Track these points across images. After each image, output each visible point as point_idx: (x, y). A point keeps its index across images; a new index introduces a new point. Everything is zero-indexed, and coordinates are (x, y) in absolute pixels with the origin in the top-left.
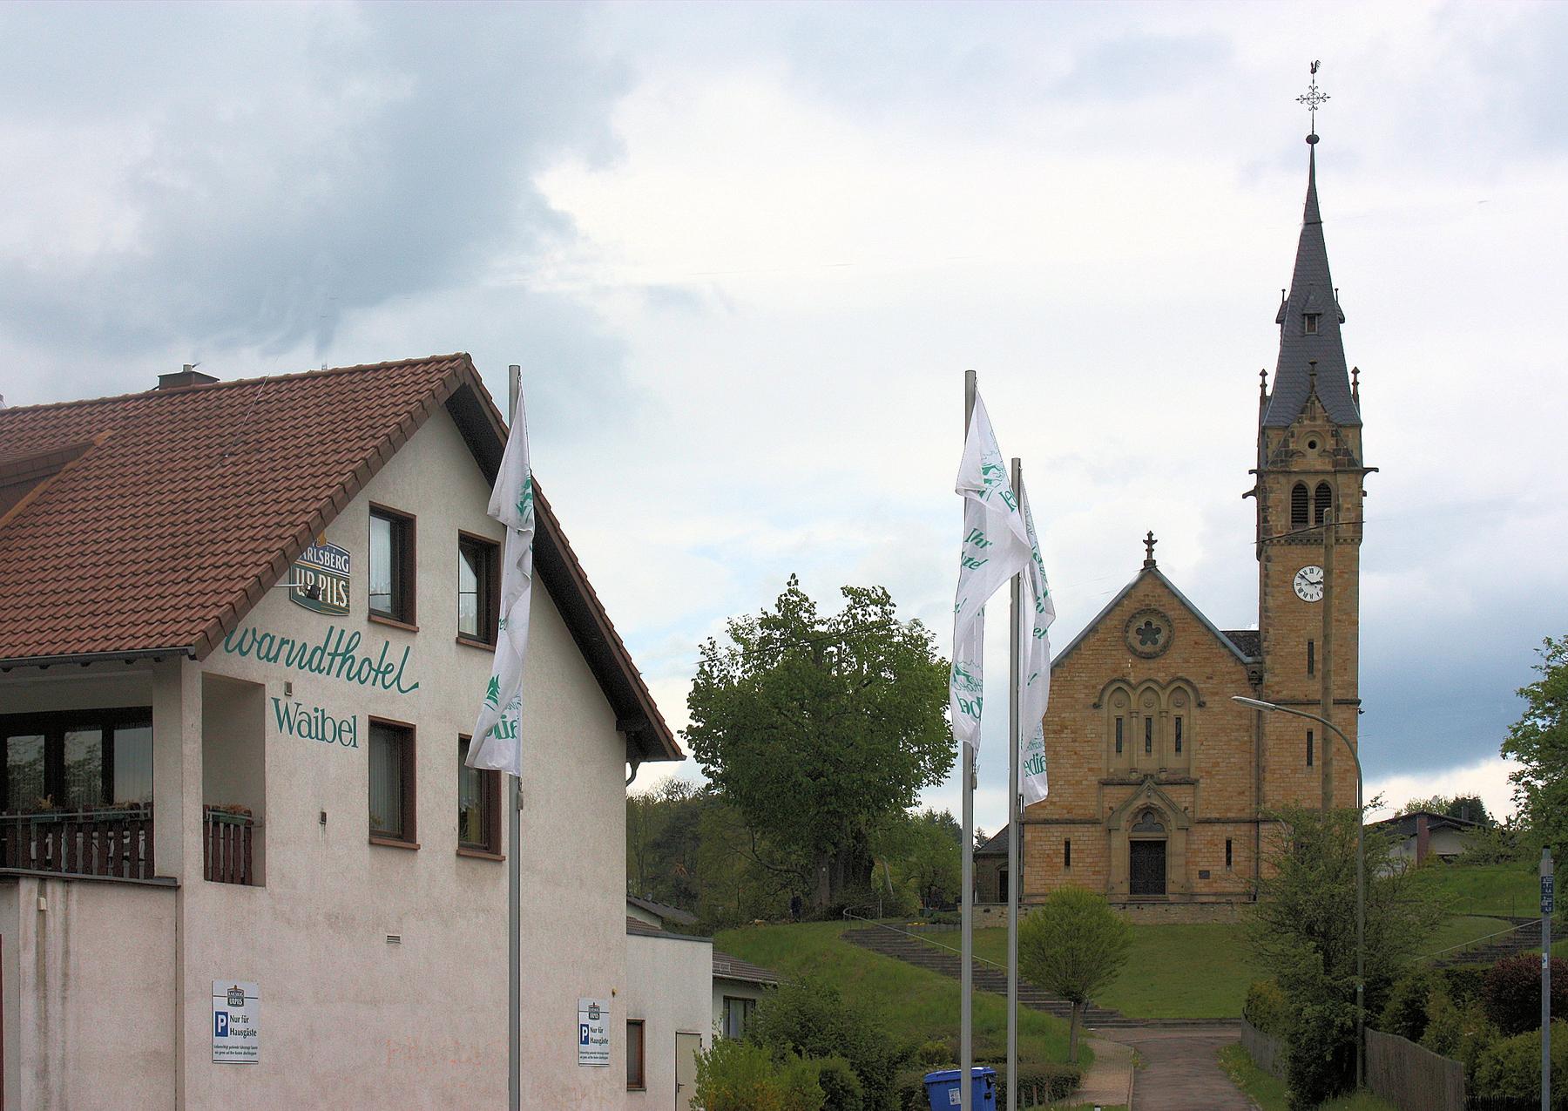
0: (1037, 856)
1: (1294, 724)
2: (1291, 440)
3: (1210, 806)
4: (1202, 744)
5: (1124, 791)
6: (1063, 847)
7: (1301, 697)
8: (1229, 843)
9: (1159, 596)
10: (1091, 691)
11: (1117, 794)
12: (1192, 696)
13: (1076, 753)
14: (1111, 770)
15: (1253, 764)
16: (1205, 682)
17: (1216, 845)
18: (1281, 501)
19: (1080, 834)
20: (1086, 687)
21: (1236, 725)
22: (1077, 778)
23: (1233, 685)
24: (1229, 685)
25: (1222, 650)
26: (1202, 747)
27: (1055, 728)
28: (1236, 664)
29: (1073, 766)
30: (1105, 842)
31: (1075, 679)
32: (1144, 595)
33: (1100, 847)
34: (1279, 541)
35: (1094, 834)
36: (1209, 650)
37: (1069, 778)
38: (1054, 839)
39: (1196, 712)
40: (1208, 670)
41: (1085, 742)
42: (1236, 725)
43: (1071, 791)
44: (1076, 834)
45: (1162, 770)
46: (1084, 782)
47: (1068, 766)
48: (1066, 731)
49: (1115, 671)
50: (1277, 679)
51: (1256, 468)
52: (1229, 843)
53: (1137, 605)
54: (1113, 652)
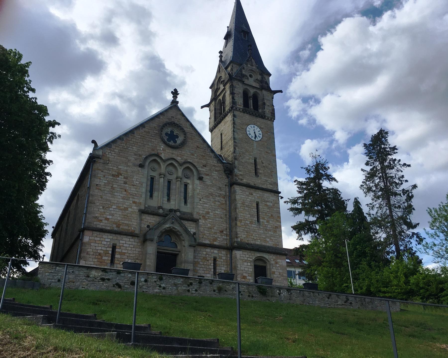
0: (92, 253)
1: (249, 198)
2: (243, 70)
3: (204, 236)
4: (200, 200)
5: (154, 219)
6: (111, 249)
7: (252, 184)
8: (215, 260)
9: (179, 119)
10: (138, 158)
11: (151, 220)
12: (195, 173)
13: (126, 191)
14: (147, 206)
15: (228, 216)
16: (202, 168)
17: (208, 261)
18: (240, 93)
19: (124, 242)
20: (135, 155)
21: (218, 193)
22: (124, 206)
23: (217, 173)
24: (214, 172)
25: (211, 154)
26: (200, 202)
27: (114, 173)
28: (218, 162)
29: (123, 198)
30: (140, 250)
31: (129, 148)
32: (172, 117)
33: (137, 252)
34: (239, 109)
35: (133, 243)
36: (204, 152)
37: (120, 205)
38: (105, 243)
39: (197, 182)
40: (204, 162)
41: (132, 185)
42: (218, 193)
43: (120, 213)
44: (121, 242)
45: (160, 207)
46: (130, 209)
47: (120, 197)
48: (120, 176)
49: (153, 150)
50: (240, 173)
51: (100, 144)
52: (215, 260)
53: (167, 120)
54: (153, 140)
